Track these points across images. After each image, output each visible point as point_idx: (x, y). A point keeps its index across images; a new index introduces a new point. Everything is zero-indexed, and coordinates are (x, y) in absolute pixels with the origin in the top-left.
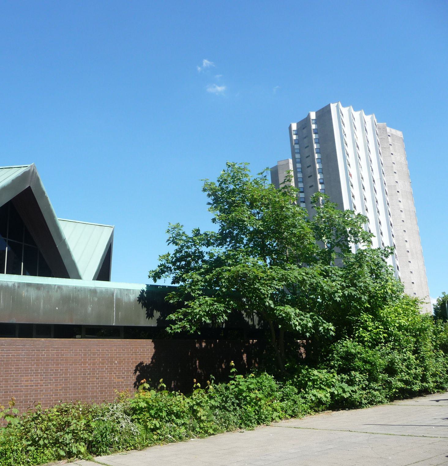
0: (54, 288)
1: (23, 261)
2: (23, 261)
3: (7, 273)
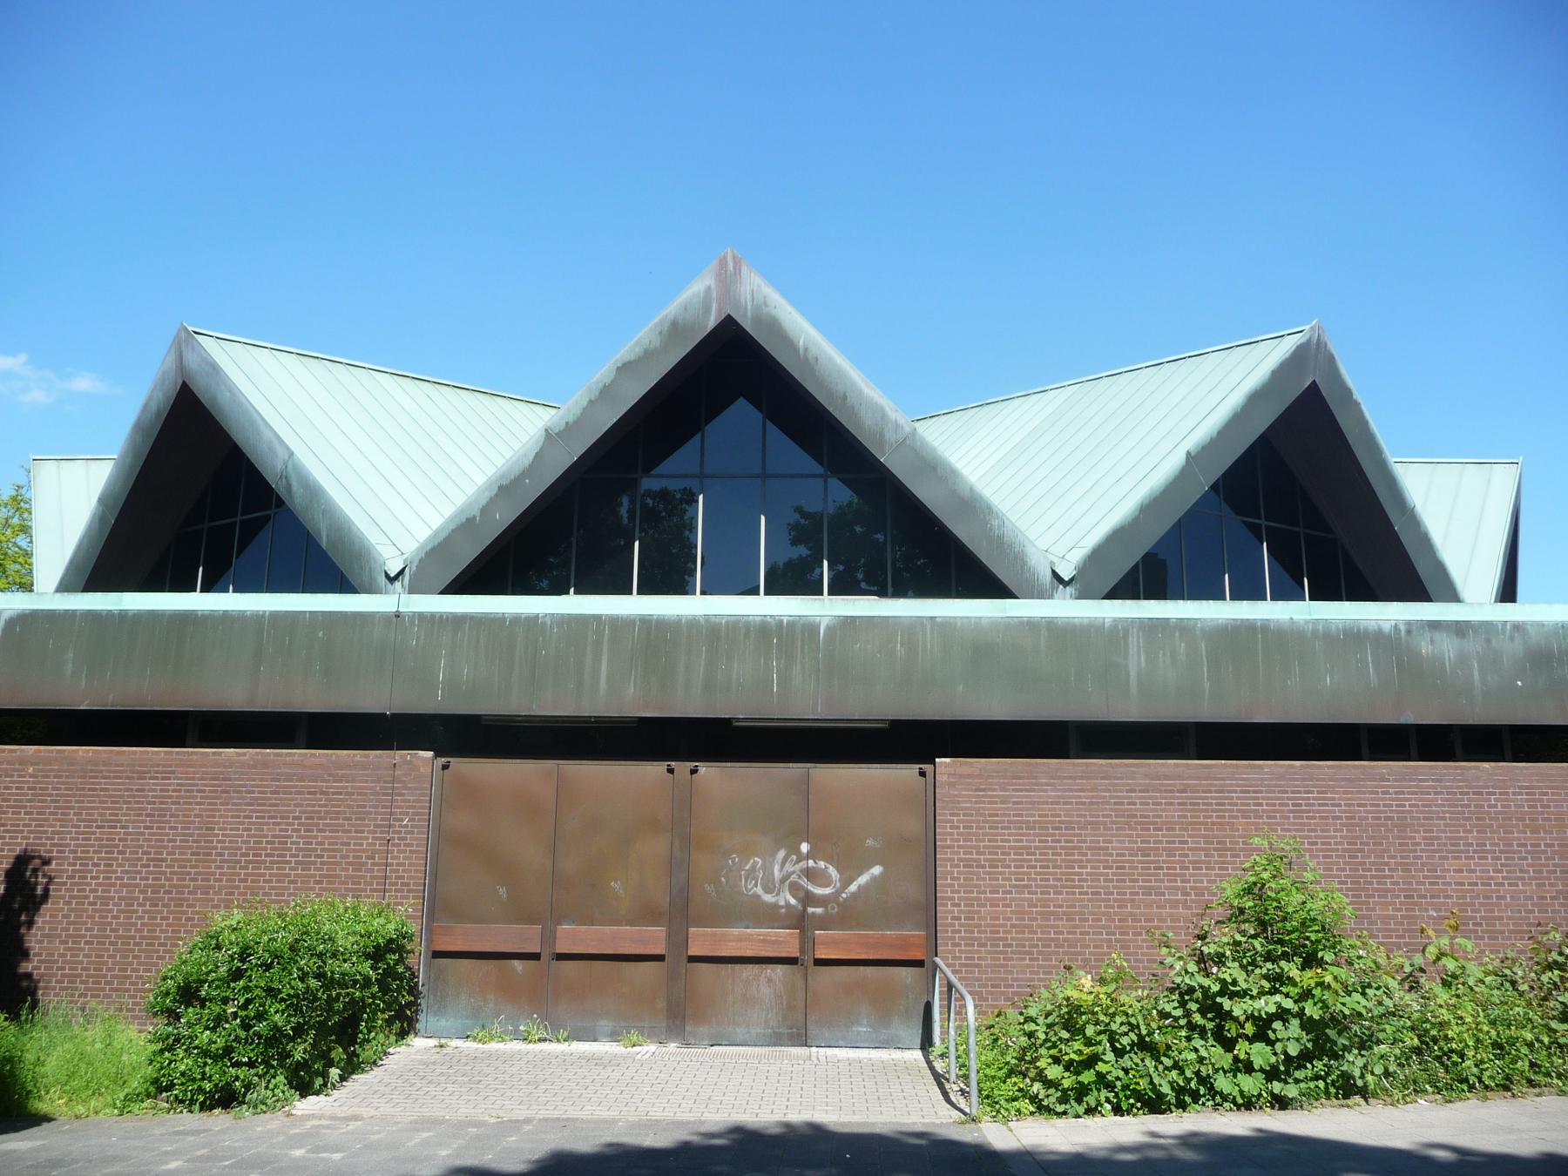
0: (305, 618)
1: (1305, 574)
2: (1305, 574)
3: (639, 593)
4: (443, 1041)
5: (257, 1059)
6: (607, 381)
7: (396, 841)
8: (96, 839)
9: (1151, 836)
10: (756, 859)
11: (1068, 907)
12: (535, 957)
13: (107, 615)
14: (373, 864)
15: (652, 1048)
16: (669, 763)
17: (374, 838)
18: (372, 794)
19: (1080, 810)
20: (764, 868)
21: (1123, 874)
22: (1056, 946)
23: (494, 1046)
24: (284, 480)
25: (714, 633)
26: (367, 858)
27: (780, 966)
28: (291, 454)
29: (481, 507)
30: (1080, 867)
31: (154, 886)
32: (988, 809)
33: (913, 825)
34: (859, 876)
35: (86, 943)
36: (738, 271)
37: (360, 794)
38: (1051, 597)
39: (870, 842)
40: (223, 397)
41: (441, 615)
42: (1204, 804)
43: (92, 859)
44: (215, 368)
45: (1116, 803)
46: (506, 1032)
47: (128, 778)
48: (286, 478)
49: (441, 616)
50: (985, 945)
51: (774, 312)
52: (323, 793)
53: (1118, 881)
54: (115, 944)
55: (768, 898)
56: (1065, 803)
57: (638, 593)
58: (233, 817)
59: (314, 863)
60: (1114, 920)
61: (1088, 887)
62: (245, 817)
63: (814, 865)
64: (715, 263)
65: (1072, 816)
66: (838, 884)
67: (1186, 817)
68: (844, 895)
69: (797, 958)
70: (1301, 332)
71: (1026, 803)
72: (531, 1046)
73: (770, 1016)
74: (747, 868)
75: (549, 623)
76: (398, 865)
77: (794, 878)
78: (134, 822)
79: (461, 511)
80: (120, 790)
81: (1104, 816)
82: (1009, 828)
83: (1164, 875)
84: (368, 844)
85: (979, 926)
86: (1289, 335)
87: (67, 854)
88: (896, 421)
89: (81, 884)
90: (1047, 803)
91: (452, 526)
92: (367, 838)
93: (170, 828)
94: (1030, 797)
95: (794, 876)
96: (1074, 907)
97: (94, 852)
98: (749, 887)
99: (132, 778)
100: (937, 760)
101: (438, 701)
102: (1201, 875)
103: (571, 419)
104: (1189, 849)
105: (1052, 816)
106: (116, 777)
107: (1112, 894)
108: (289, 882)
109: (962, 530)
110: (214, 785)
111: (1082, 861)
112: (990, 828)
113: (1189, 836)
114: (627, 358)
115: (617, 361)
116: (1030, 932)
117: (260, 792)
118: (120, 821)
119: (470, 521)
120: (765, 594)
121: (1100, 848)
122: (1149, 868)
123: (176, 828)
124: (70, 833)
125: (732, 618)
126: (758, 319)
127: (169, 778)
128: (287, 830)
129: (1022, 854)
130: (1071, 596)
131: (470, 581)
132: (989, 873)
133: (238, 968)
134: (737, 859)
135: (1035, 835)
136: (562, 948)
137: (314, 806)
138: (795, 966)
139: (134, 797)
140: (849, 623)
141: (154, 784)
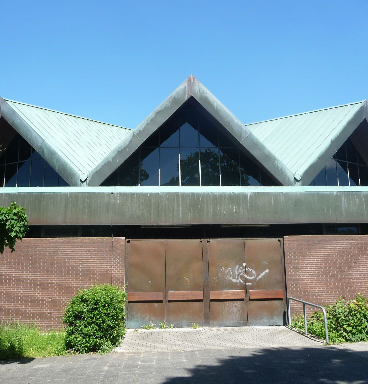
0: (81, 195)
1: (359, 178)
2: (359, 178)
3: (222, 185)
4: (137, 329)
5: (102, 336)
6: (153, 117)
7: (114, 266)
8: (13, 268)
9: (349, 258)
10: (230, 268)
11: (326, 280)
12: (161, 302)
13: (14, 194)
14: (107, 274)
15: (201, 329)
16: (279, 238)
17: (107, 265)
18: (105, 251)
19: (328, 251)
20: (232, 271)
21: (342, 270)
22: (323, 293)
23: (151, 330)
24: (41, 149)
25: (216, 198)
26: (105, 272)
27: (239, 302)
28: (44, 141)
29: (112, 158)
30: (329, 268)
31: (34, 283)
32: (301, 251)
33: (277, 256)
34: (262, 273)
35: (12, 302)
36: (194, 82)
37: (101, 251)
38: (294, 185)
39: (265, 262)
40: (17, 122)
41: (127, 193)
42: (364, 248)
43: (12, 275)
44: (14, 112)
45: (338, 248)
46: (154, 326)
47: (22, 248)
48: (42, 149)
49: (127, 194)
50: (301, 293)
51: (206, 95)
52: (89, 251)
53: (340, 272)
54: (30, 302)
55: (234, 281)
56: (323, 249)
57: (361, 186)
58: (59, 260)
59: (88, 274)
60: (339, 284)
61: (331, 274)
62: (63, 260)
63: (248, 270)
64: (187, 79)
65: (326, 253)
66: (255, 276)
67: (359, 252)
68: (257, 279)
69: (244, 299)
70: (362, 102)
71: (312, 249)
72: (163, 330)
73: (236, 317)
74: (227, 271)
75: (162, 195)
76: (116, 274)
77: (241, 274)
78: (26, 262)
79: (106, 159)
80: (20, 252)
81: (335, 252)
82: (307, 257)
83: (354, 270)
84: (105, 267)
85: (300, 287)
86: (356, 103)
87: (3, 274)
88: (245, 130)
89: (9, 283)
90: (318, 249)
91: (102, 164)
92: (105, 266)
93: (38, 264)
94: (313, 247)
95: (242, 273)
96: (328, 280)
97: (13, 273)
98: (228, 277)
99: (24, 248)
100: (284, 236)
101: (127, 221)
102: (365, 269)
103: (141, 129)
104: (361, 262)
105: (320, 253)
106: (19, 248)
107: (339, 276)
108: (80, 280)
109: (266, 165)
110: (52, 250)
111: (329, 266)
112: (301, 257)
113: (360, 258)
114: (159, 110)
115: (156, 111)
116: (315, 289)
117: (68, 252)
118: (21, 262)
119: (109, 162)
120: (181, 186)
121: (334, 262)
122: (349, 268)
123: (40, 264)
124: (4, 266)
125: (220, 193)
126: (201, 98)
127: (37, 248)
128: (78, 264)
129: (311, 265)
130: (300, 185)
131: (107, 183)
132: (302, 271)
133: (95, 307)
134: (224, 269)
135: (315, 259)
136: (170, 299)
137: (86, 255)
138: (243, 302)
139: (25, 254)
140: (257, 194)
141: (32, 250)
